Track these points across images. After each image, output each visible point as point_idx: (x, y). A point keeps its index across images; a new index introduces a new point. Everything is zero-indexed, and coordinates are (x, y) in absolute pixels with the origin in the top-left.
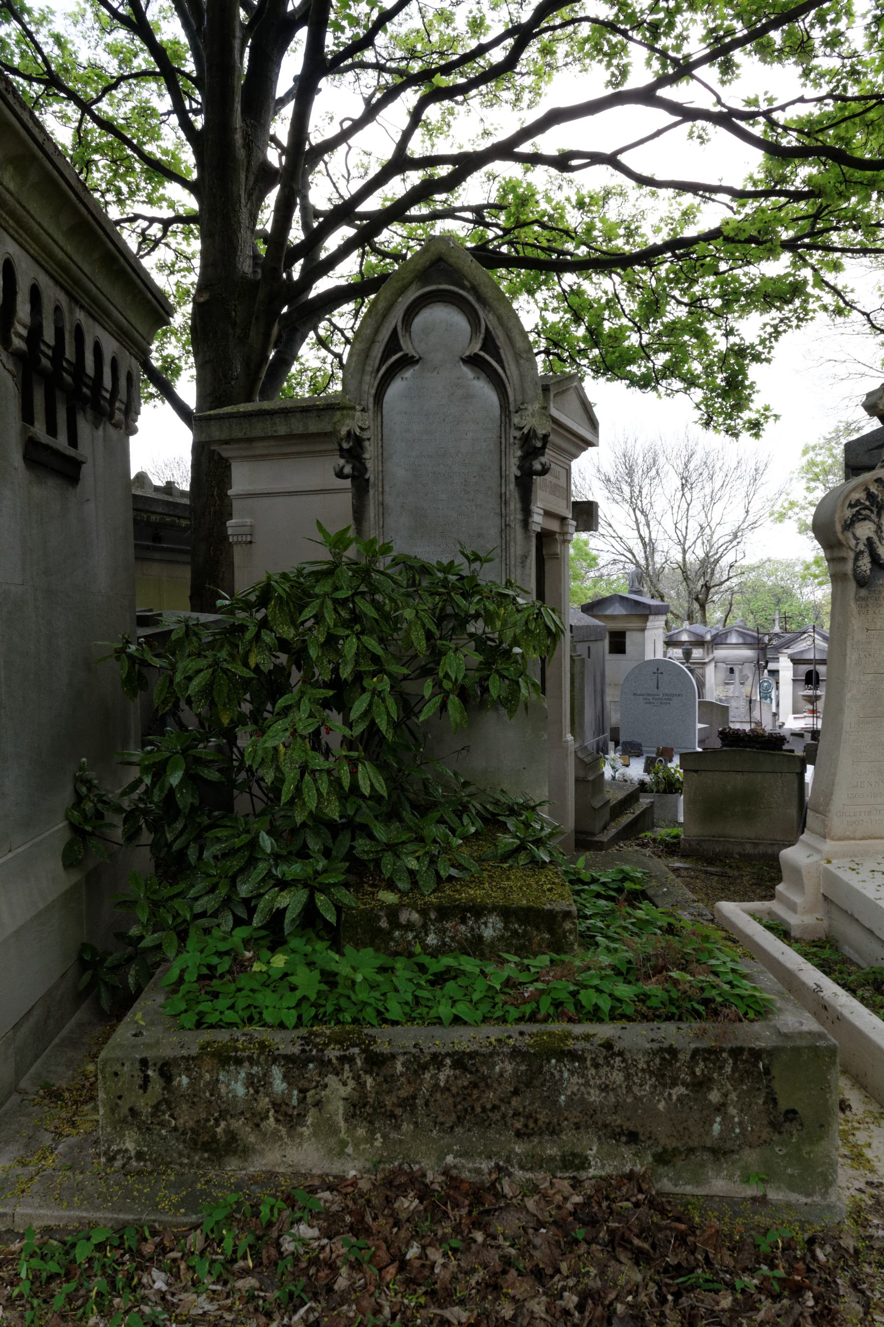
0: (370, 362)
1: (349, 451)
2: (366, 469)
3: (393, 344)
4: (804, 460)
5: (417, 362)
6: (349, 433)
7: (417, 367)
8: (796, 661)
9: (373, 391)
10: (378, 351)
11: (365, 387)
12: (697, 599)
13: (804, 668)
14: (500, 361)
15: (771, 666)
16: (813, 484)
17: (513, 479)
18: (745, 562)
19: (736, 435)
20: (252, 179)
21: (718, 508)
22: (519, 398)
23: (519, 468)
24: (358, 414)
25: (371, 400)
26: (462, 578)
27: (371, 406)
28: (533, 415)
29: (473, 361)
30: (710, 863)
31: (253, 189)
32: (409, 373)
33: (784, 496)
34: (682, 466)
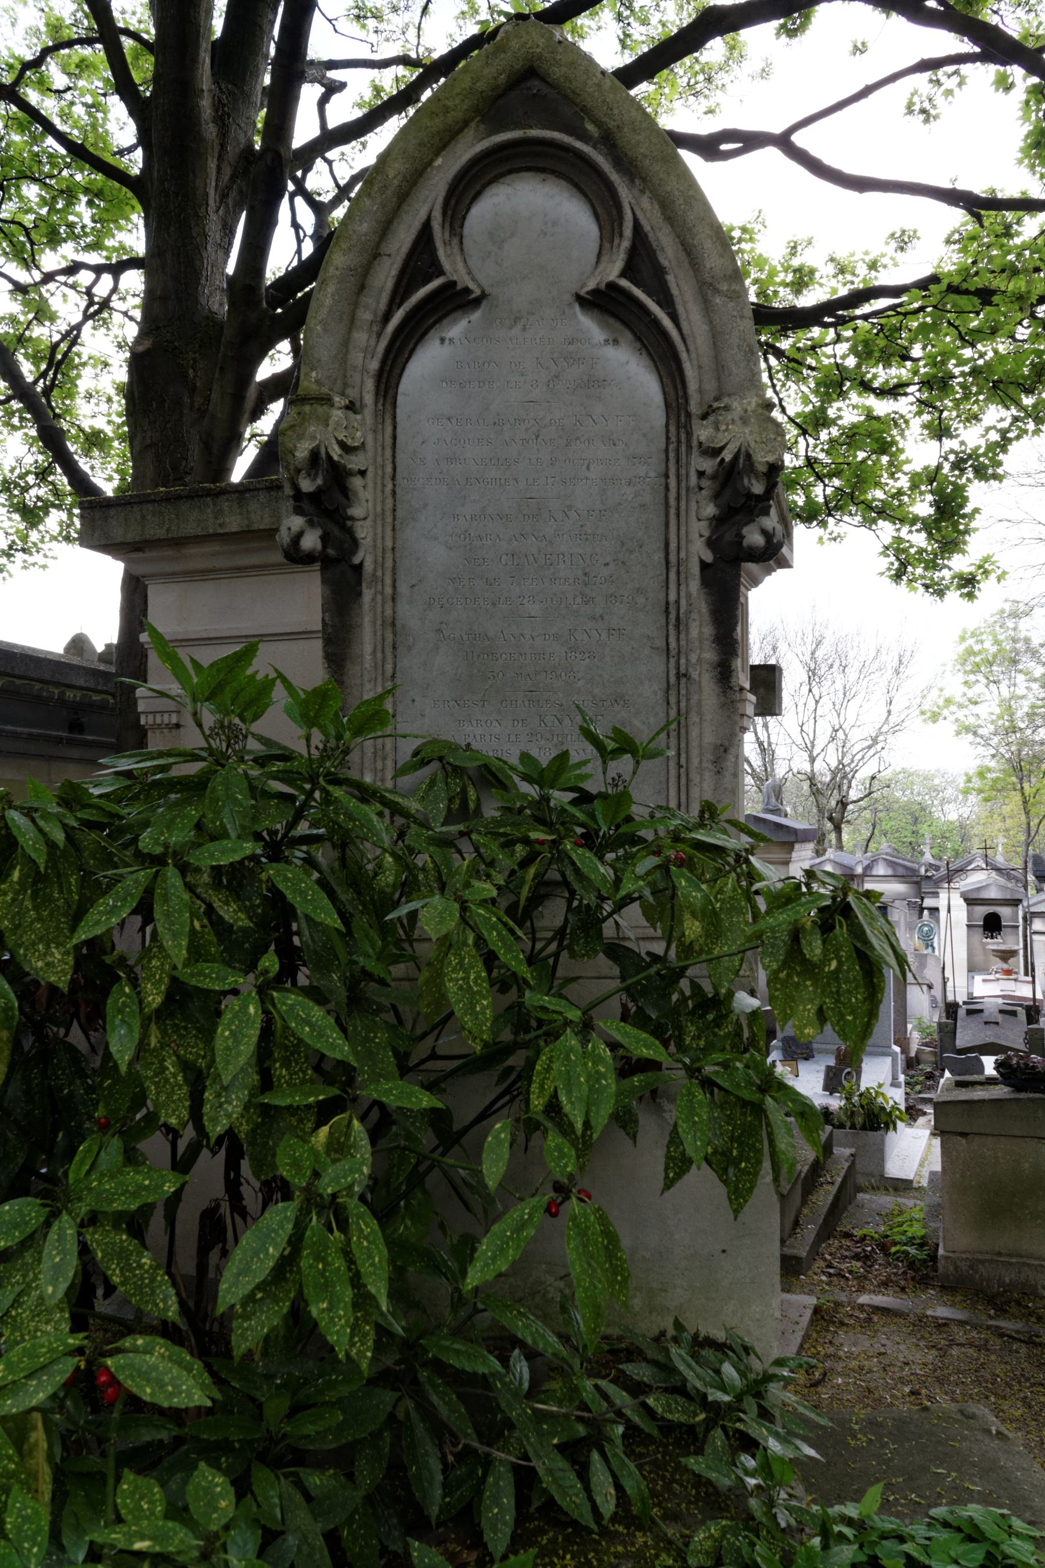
0: (367, 300)
1: (315, 497)
2: (355, 543)
3: (422, 260)
4: (961, 648)
5: (477, 302)
6: (315, 456)
7: (476, 316)
8: (971, 901)
9: (374, 365)
10: (386, 275)
11: (357, 357)
12: (831, 819)
13: (982, 911)
14: (667, 302)
15: (928, 902)
16: (972, 678)
17: (695, 569)
18: (886, 774)
19: (940, 594)
20: (227, 171)
21: (853, 705)
22: (710, 387)
23: (711, 543)
24: (337, 414)
25: (370, 384)
26: (584, 798)
27: (369, 399)
28: (745, 421)
29: (604, 302)
30: (1002, 1311)
31: (229, 188)
32: (457, 328)
33: (935, 692)
34: (807, 657)
